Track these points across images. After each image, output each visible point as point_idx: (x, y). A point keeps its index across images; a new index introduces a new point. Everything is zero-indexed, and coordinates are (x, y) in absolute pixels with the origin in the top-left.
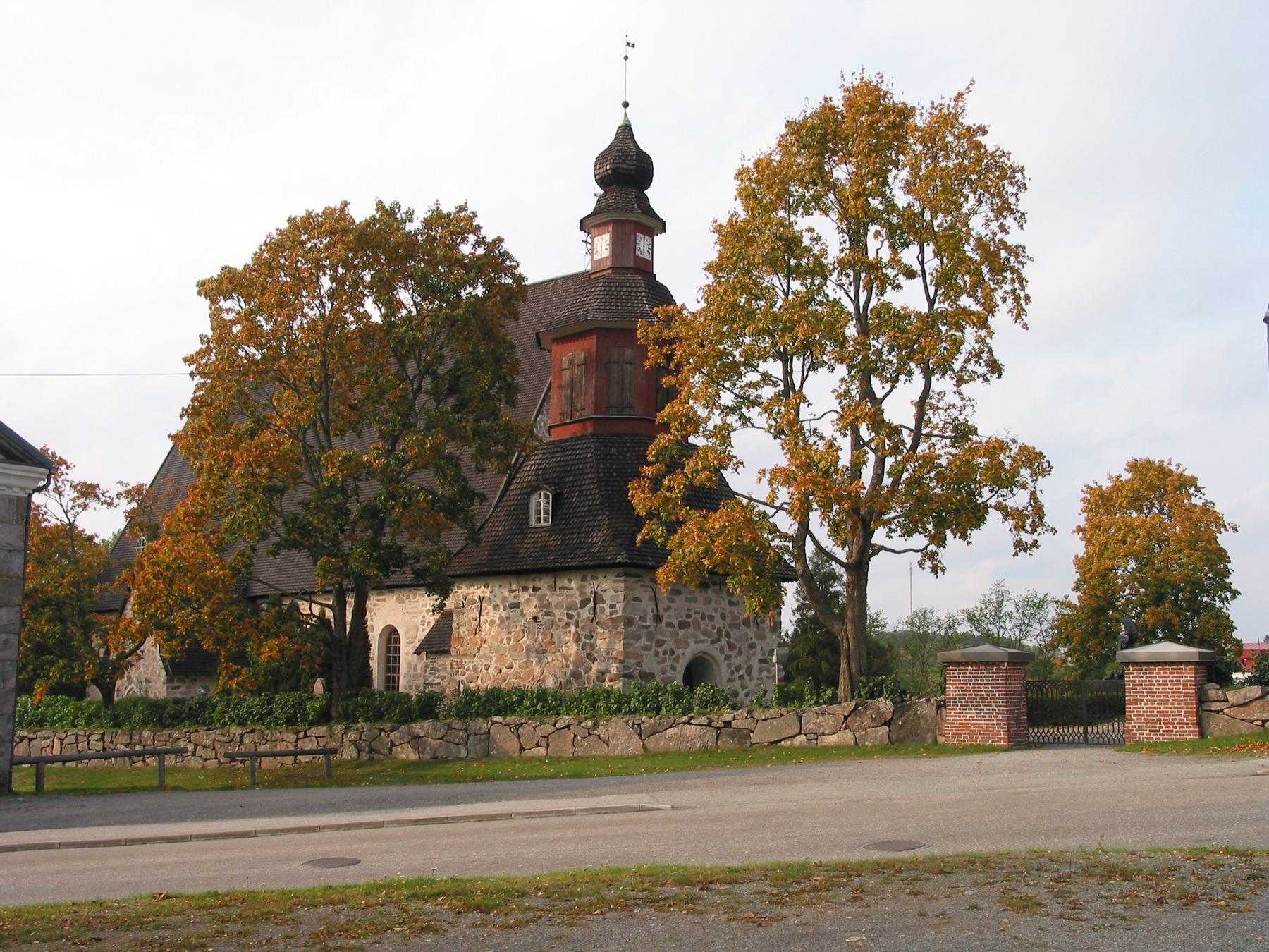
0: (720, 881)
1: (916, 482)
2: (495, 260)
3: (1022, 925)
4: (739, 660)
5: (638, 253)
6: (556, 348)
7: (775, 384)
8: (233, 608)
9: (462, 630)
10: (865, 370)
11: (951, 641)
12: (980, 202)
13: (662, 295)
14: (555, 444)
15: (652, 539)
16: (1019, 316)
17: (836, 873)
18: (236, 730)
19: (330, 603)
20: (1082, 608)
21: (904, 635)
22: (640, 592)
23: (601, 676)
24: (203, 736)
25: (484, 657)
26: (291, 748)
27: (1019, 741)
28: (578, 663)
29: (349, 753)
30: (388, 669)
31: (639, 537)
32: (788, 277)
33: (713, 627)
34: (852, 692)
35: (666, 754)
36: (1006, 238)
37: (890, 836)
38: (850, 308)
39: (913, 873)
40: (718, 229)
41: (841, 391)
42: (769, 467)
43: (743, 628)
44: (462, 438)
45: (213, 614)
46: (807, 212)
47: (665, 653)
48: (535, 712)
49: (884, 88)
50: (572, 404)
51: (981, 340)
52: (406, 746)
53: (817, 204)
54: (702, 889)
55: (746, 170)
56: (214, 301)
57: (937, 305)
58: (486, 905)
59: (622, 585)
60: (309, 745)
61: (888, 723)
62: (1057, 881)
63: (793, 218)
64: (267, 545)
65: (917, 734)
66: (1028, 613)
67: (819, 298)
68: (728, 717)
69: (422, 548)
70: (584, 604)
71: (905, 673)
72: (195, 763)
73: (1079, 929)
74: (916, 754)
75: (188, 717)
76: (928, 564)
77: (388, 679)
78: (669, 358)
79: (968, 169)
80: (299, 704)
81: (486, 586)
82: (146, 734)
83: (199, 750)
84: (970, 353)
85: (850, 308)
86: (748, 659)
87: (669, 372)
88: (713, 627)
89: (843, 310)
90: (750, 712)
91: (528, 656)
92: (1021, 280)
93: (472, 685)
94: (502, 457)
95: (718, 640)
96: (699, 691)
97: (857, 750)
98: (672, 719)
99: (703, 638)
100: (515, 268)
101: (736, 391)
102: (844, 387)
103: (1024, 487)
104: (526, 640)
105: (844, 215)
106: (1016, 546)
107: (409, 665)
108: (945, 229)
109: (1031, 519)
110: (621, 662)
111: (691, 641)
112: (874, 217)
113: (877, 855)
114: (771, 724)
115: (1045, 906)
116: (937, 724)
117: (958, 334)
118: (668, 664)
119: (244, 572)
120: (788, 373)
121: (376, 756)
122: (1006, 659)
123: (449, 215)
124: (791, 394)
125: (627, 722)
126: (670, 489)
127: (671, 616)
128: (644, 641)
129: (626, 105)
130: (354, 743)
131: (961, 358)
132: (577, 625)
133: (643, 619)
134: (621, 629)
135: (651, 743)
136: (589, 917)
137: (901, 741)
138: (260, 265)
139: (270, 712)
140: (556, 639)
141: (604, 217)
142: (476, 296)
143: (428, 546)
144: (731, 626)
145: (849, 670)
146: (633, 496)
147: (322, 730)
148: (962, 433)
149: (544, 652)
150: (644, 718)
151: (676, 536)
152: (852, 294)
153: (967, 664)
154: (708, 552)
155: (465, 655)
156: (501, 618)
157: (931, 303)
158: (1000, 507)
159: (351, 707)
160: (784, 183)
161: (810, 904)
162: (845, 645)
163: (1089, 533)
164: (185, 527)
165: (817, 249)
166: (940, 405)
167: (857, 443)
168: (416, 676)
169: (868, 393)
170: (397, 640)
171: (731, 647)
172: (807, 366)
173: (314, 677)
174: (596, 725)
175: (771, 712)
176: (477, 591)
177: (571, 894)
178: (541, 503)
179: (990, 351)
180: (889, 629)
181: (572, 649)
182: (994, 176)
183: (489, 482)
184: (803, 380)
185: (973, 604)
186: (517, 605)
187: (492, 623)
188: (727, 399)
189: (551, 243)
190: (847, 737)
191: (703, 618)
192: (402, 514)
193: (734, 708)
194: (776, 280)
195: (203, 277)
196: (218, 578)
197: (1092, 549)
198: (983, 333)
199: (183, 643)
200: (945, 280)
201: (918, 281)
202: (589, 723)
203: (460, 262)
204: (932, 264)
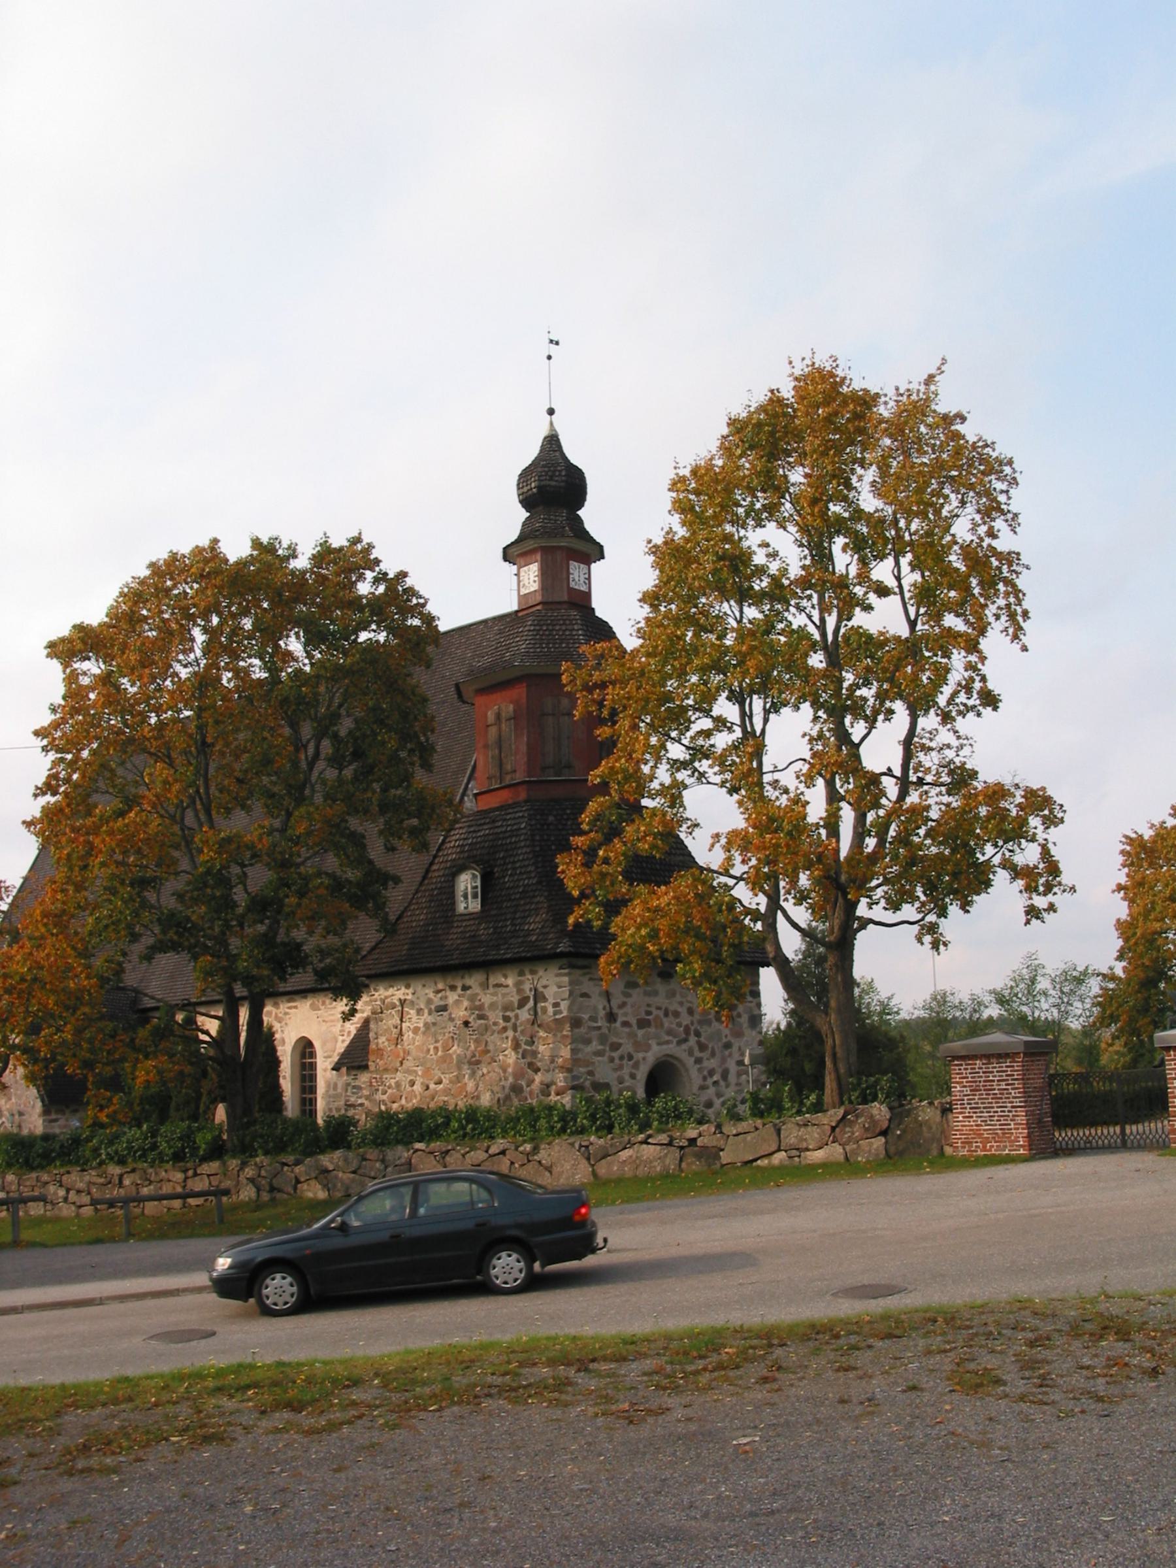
0: (605, 1359)
1: (903, 839)
2: (398, 598)
3: (967, 1414)
4: (712, 1063)
5: (572, 584)
6: (480, 701)
7: (730, 730)
8: (100, 1024)
9: (382, 1040)
10: (839, 710)
11: (977, 1027)
12: (963, 503)
13: (603, 631)
14: (483, 813)
15: (589, 921)
16: (1016, 637)
17: (755, 1342)
18: (115, 1170)
19: (220, 1014)
20: (1128, 981)
21: (920, 1021)
22: (587, 986)
23: (546, 1088)
24: (75, 1178)
25: (408, 1071)
26: (179, 1190)
27: (1043, 1147)
28: (518, 1075)
29: (247, 1193)
30: (304, 1090)
31: (571, 920)
32: (740, 604)
33: (679, 1025)
34: (841, 1095)
35: (619, 1181)
36: (995, 543)
37: (866, 1280)
38: (817, 636)
39: (853, 1339)
40: (654, 550)
41: (814, 733)
42: (725, 829)
43: (715, 1024)
44: (366, 812)
45: (78, 1032)
46: (759, 524)
47: (621, 1058)
48: (465, 1135)
49: (840, 373)
50: (501, 765)
51: (970, 667)
52: (313, 1182)
53: (771, 515)
54: (579, 1370)
55: (682, 480)
56: (66, 665)
57: (919, 627)
58: (300, 1401)
59: (566, 979)
60: (199, 1185)
61: (884, 1133)
62: (1031, 1344)
63: (742, 532)
64: (138, 948)
65: (920, 1146)
66: (1066, 990)
67: (780, 626)
68: (692, 1133)
69: (324, 944)
70: (522, 1003)
71: (898, 1069)
72: (67, 1211)
73: (1038, 1417)
74: (918, 1170)
75: (59, 1156)
76: (927, 939)
77: (303, 1102)
78: (600, 704)
79: (942, 461)
80: (188, 1137)
81: (408, 987)
82: (10, 1177)
83: (72, 1196)
84: (959, 684)
85: (817, 636)
86: (724, 1060)
87: (602, 722)
88: (679, 1025)
89: (809, 636)
90: (719, 1126)
91: (459, 1068)
92: (1017, 592)
93: (395, 1106)
94: (414, 832)
95: (686, 1040)
96: (659, 1104)
97: (848, 1168)
98: (626, 1138)
99: (667, 1038)
100: (423, 605)
101: (685, 742)
102: (817, 728)
103: (1033, 839)
104: (456, 1050)
105: (804, 529)
106: (1027, 913)
107: (328, 1085)
108: (922, 537)
109: (1043, 878)
110: (569, 1070)
111: (653, 1043)
112: (838, 526)
113: (847, 1308)
114: (742, 1142)
115: (1005, 1383)
116: (943, 1132)
117: (944, 661)
118: (626, 1071)
119: (112, 981)
120: (746, 716)
121: (278, 1195)
122: (1021, 1049)
123: (341, 549)
124: (753, 744)
125: (572, 1145)
126: (606, 861)
127: (626, 1014)
128: (595, 1046)
129: (551, 412)
130: (252, 1180)
131: (947, 690)
132: (515, 1029)
133: (593, 1019)
134: (566, 1031)
135: (602, 1169)
136: (422, 1415)
137: (900, 1154)
138: (118, 619)
139: (154, 1147)
140: (491, 1047)
141: (530, 544)
142: (377, 641)
143: (333, 940)
144: (700, 1022)
145: (836, 1070)
146: (563, 872)
147: (214, 1166)
148: (961, 778)
149: (478, 1062)
150: (592, 1138)
151: (619, 918)
152: (816, 619)
153: (974, 1057)
154: (654, 935)
155: (386, 1070)
156: (426, 1025)
157: (912, 624)
158: (1007, 865)
159: (248, 1139)
160: (729, 491)
161: (709, 1388)
162: (830, 1041)
163: (1132, 890)
164: (43, 930)
165: (774, 567)
166: (933, 745)
167: (833, 797)
168: (336, 1097)
169: (843, 736)
170: (312, 1055)
171: (702, 1047)
172: (768, 706)
173: (214, 1102)
174: (536, 1149)
175: (743, 1126)
176: (397, 993)
177: (414, 1382)
178: (466, 882)
179: (984, 679)
180: (904, 1015)
181: (511, 1058)
182: (978, 471)
183: (406, 864)
184: (766, 721)
185: (1001, 981)
186: (444, 1008)
187: (416, 1030)
188: (676, 751)
189: (469, 582)
190: (834, 1152)
191: (666, 1014)
192: (299, 905)
193: (700, 1122)
194: (727, 608)
195: (53, 637)
196: (82, 990)
197: (1136, 909)
198: (973, 658)
199: (46, 1068)
200: (924, 594)
201: (895, 600)
202: (528, 1147)
203: (355, 603)
204: (911, 578)
